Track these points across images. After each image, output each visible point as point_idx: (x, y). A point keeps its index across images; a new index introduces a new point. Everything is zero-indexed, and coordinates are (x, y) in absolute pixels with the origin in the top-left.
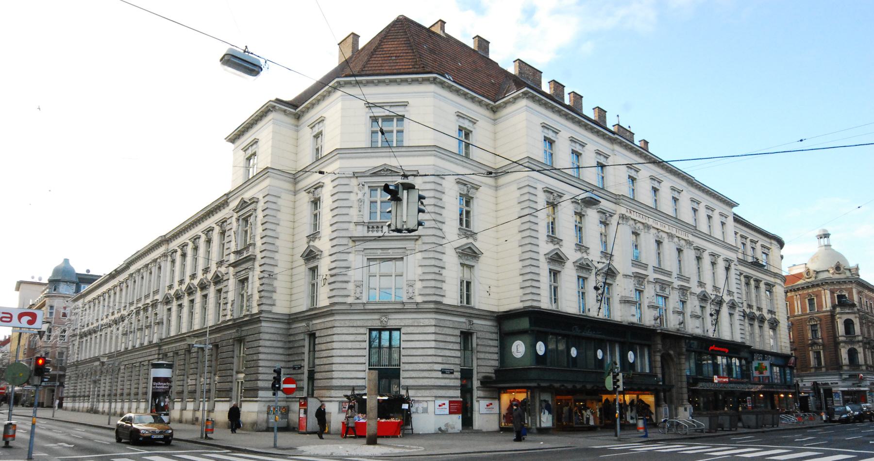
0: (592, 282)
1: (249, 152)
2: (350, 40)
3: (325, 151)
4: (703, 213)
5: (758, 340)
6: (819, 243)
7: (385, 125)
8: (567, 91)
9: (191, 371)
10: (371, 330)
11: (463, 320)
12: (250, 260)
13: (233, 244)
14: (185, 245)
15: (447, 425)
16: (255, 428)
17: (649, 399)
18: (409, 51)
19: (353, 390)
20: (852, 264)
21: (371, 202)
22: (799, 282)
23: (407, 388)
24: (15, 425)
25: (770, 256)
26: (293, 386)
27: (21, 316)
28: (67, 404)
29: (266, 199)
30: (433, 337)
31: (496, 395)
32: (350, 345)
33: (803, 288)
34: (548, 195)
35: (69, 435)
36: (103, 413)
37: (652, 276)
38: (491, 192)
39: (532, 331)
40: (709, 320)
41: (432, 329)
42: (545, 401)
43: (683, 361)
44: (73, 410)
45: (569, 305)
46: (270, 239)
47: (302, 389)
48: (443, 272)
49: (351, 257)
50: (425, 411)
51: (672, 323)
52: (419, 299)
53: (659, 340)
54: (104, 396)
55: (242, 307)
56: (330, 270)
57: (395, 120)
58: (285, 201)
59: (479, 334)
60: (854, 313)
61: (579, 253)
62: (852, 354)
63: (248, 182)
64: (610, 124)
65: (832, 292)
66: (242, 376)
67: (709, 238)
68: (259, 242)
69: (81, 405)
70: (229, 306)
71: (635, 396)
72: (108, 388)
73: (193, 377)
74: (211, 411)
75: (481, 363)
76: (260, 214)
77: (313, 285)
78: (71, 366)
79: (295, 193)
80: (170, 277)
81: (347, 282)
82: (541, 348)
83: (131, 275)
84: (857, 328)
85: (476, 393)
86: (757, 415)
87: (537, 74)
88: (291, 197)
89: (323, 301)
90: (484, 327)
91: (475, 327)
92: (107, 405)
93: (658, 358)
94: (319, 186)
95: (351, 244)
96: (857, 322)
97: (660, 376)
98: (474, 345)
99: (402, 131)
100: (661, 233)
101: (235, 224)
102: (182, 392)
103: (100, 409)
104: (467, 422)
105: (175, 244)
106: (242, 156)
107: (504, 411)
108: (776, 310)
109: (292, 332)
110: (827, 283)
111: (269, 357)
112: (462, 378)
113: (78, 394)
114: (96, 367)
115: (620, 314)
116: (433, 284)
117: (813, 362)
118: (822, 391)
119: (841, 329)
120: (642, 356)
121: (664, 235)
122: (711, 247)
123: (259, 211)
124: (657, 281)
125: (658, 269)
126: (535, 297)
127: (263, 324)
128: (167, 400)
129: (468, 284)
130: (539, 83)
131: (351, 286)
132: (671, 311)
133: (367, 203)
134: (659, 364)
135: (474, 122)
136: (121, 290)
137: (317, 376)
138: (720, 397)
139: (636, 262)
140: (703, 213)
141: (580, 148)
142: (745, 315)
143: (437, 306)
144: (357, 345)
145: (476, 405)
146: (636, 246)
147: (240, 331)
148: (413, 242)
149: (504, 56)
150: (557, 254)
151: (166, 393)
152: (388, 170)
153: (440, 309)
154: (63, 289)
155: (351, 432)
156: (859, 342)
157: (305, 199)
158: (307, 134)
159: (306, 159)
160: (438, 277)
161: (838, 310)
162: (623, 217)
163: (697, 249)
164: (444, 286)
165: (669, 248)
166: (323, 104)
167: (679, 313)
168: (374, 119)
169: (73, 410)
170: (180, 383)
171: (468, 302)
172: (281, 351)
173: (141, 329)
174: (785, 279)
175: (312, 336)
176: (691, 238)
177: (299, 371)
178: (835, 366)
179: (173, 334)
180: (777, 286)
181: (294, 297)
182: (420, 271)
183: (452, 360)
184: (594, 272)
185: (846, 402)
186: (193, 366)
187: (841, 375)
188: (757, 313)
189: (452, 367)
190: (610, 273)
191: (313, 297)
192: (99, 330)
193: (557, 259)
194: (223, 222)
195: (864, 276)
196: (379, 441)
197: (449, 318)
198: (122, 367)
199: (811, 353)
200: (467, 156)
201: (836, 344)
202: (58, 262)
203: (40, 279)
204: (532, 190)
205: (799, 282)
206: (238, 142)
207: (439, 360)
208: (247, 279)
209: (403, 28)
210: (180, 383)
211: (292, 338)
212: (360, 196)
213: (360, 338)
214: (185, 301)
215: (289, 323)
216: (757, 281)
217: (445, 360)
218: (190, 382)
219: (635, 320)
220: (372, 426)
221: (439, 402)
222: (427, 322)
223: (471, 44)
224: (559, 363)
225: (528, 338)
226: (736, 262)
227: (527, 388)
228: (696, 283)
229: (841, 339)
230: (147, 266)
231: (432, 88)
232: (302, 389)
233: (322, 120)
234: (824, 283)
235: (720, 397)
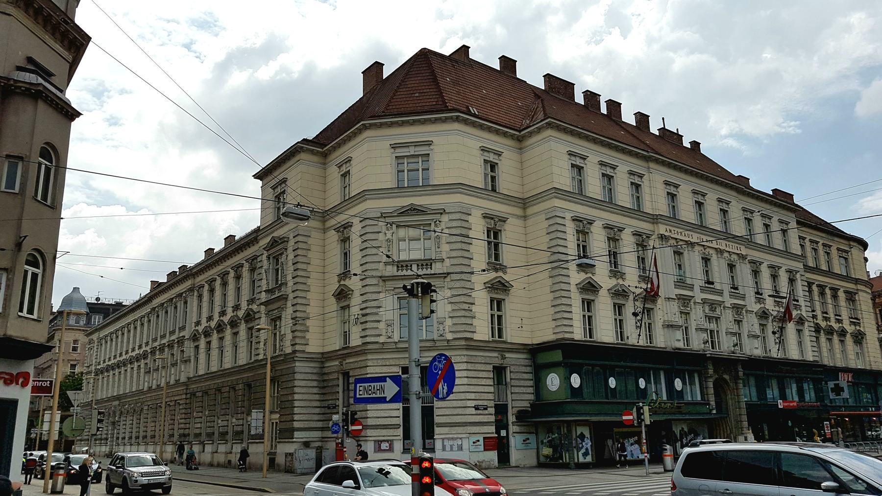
0: (629, 308)
1: (279, 190)
4: (758, 224)
11: (495, 354)
13: (264, 282)
34: (609, 231)
37: (699, 296)
38: (519, 222)
40: (771, 339)
48: (474, 308)
49: (382, 295)
51: (726, 346)
52: (450, 336)
54: (124, 438)
56: (361, 309)
61: (614, 279)
70: (262, 344)
75: (515, 397)
79: (325, 230)
81: (379, 321)
83: (154, 309)
85: (512, 428)
87: (568, 87)
89: (355, 341)
91: (506, 361)
93: (711, 385)
94: (347, 226)
95: (381, 283)
97: (713, 403)
98: (508, 380)
100: (708, 250)
101: (265, 263)
104: (504, 460)
109: (326, 370)
111: (305, 397)
112: (496, 414)
114: (115, 407)
115: (663, 340)
120: (692, 383)
121: (712, 252)
122: (768, 259)
123: (290, 250)
124: (704, 302)
131: (382, 325)
132: (694, 328)
134: (711, 391)
135: (499, 154)
139: (681, 283)
140: (758, 224)
142: (818, 329)
146: (680, 266)
153: (471, 345)
157: (333, 237)
158: (334, 173)
162: (662, 237)
163: (752, 262)
167: (734, 334)
171: (500, 337)
176: (744, 251)
181: (327, 336)
182: (449, 308)
183: (486, 396)
184: (631, 297)
188: (836, 326)
189: (485, 403)
193: (590, 288)
194: (255, 258)
197: (481, 354)
198: (146, 408)
207: (472, 396)
208: (280, 318)
211: (326, 377)
216: (822, 287)
217: (478, 396)
219: (680, 345)
224: (585, 397)
225: (561, 370)
228: (753, 299)
231: (456, 126)
233: (349, 160)
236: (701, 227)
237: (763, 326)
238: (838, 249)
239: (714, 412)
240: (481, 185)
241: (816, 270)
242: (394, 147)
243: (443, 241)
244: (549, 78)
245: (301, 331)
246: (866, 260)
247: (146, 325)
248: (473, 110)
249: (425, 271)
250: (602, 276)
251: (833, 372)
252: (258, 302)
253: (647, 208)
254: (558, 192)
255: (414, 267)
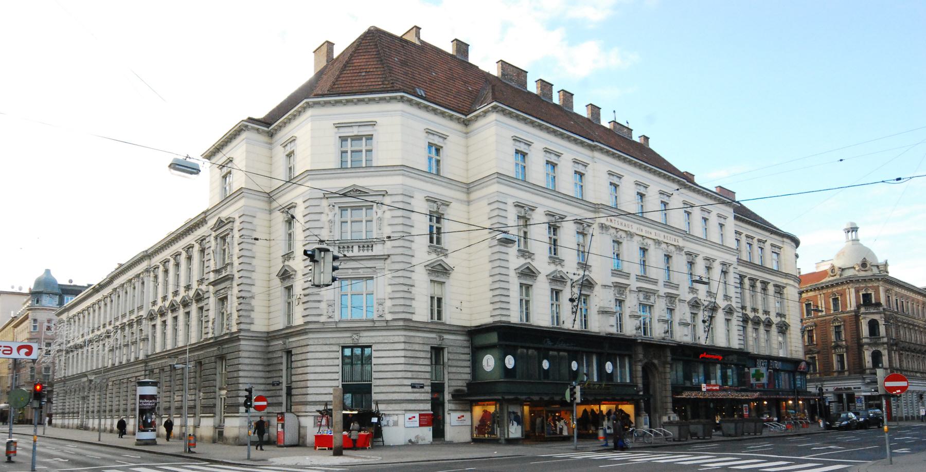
0: (566, 294)
1: (225, 170)
2: (325, 48)
3: (298, 172)
5: (763, 344)
6: (847, 237)
7: (355, 145)
8: (555, 90)
9: (177, 388)
10: (343, 347)
11: (433, 335)
12: (228, 279)
13: (212, 262)
14: (166, 262)
15: (417, 437)
16: (238, 442)
17: (629, 409)
18: (382, 66)
19: (326, 405)
20: (881, 260)
21: (342, 222)
22: (824, 281)
23: (377, 403)
24: (15, 442)
25: (782, 256)
26: (265, 403)
27: (19, 348)
28: (57, 421)
29: (242, 219)
30: (402, 353)
31: (468, 407)
32: (323, 362)
33: (827, 287)
34: (519, 209)
35: (62, 451)
36: (93, 429)
37: (634, 284)
38: (464, 207)
39: (501, 345)
40: (701, 327)
41: (402, 346)
42: (514, 413)
43: (668, 370)
44: (63, 427)
45: (541, 318)
46: (247, 259)
47: (280, 404)
50: (396, 424)
51: (657, 332)
52: (389, 317)
53: (640, 350)
54: (93, 412)
55: (223, 325)
57: (364, 139)
58: (260, 221)
59: (450, 349)
60: (880, 313)
62: (876, 357)
63: (227, 199)
64: (605, 122)
65: (857, 291)
66: (224, 392)
67: (704, 241)
68: (236, 262)
69: (71, 421)
70: (210, 324)
71: (613, 407)
72: (97, 404)
73: (179, 393)
74: (196, 426)
75: (452, 376)
76: (237, 235)
77: (289, 303)
78: (58, 382)
79: (271, 212)
80: (153, 295)
81: (319, 301)
82: (510, 362)
83: (115, 290)
84: (882, 330)
85: (448, 406)
86: (736, 424)
87: (521, 74)
88: (266, 216)
89: (298, 320)
90: (456, 344)
92: (97, 421)
93: (639, 368)
94: (292, 206)
96: (882, 323)
97: (640, 385)
98: (446, 360)
99: (371, 151)
100: (646, 240)
101: (213, 243)
102: (169, 408)
103: (90, 425)
104: (439, 434)
105: (157, 260)
106: (218, 174)
107: (476, 423)
108: (786, 313)
109: (271, 349)
110: (851, 281)
112: (433, 392)
113: (67, 410)
115: (599, 325)
116: (402, 302)
117: (836, 365)
118: (844, 396)
119: (865, 330)
120: (622, 366)
121: (650, 242)
124: (640, 290)
125: (643, 278)
126: (504, 312)
127: (242, 342)
128: (154, 416)
129: (439, 300)
130: (524, 84)
131: (323, 305)
132: (657, 318)
133: (338, 224)
134: (640, 374)
135: (444, 137)
136: (106, 304)
137: (294, 392)
138: (712, 405)
141: (556, 158)
142: (745, 319)
143: (406, 324)
144: (330, 362)
145: (447, 417)
147: (219, 350)
148: (383, 261)
149: (485, 60)
150: (528, 268)
151: (152, 410)
152: (357, 190)
153: (410, 326)
154: (46, 301)
155: (322, 442)
156: (884, 343)
158: (280, 153)
159: (281, 173)
160: (407, 295)
161: (863, 310)
162: (603, 227)
163: (689, 254)
164: (414, 303)
165: (655, 257)
166: (295, 123)
167: (666, 321)
168: (343, 139)
169: (63, 427)
170: (168, 399)
171: (439, 318)
172: (260, 368)
173: (127, 345)
174: (799, 279)
175: (289, 353)
176: (681, 243)
177: (278, 387)
178: (858, 370)
179: (158, 350)
180: (788, 287)
181: (272, 315)
182: (389, 289)
185: (869, 407)
186: (178, 382)
187: (864, 379)
188: (763, 317)
189: (422, 382)
190: (588, 284)
191: (289, 316)
192: (85, 345)
193: (528, 273)
194: (202, 240)
195: (893, 273)
196: (344, 452)
198: (110, 383)
199: (834, 357)
200: (438, 174)
201: (860, 346)
202: (39, 273)
203: (20, 289)
204: (502, 206)
205: (824, 281)
206: (214, 160)
207: (409, 375)
208: (226, 298)
209: (375, 42)
210: (168, 399)
211: (270, 356)
212: (331, 217)
213: (333, 355)
214: (169, 318)
215: (268, 341)
216: (765, 284)
218: (177, 398)
219: (614, 330)
220: (337, 441)
221: (410, 415)
222: (396, 339)
223: (449, 49)
224: (531, 373)
225: (496, 352)
226: (735, 265)
227: (497, 401)
229: (865, 341)
230: (130, 281)
231: (400, 106)
232: (280, 404)
233: (293, 140)
234: (850, 281)
235: (712, 405)
236: (640, 217)
237: (694, 315)
238: (772, 245)
239: (641, 393)
240: (425, 168)
241: (751, 265)
242: (338, 126)
243: (385, 222)
244: (504, 64)
245: (246, 310)
246: (797, 256)
247: (109, 305)
248: (421, 92)
249: (366, 253)
250: (542, 264)
251: (754, 359)
252: (207, 282)
253: (590, 197)
254: (500, 177)
255: (356, 248)
